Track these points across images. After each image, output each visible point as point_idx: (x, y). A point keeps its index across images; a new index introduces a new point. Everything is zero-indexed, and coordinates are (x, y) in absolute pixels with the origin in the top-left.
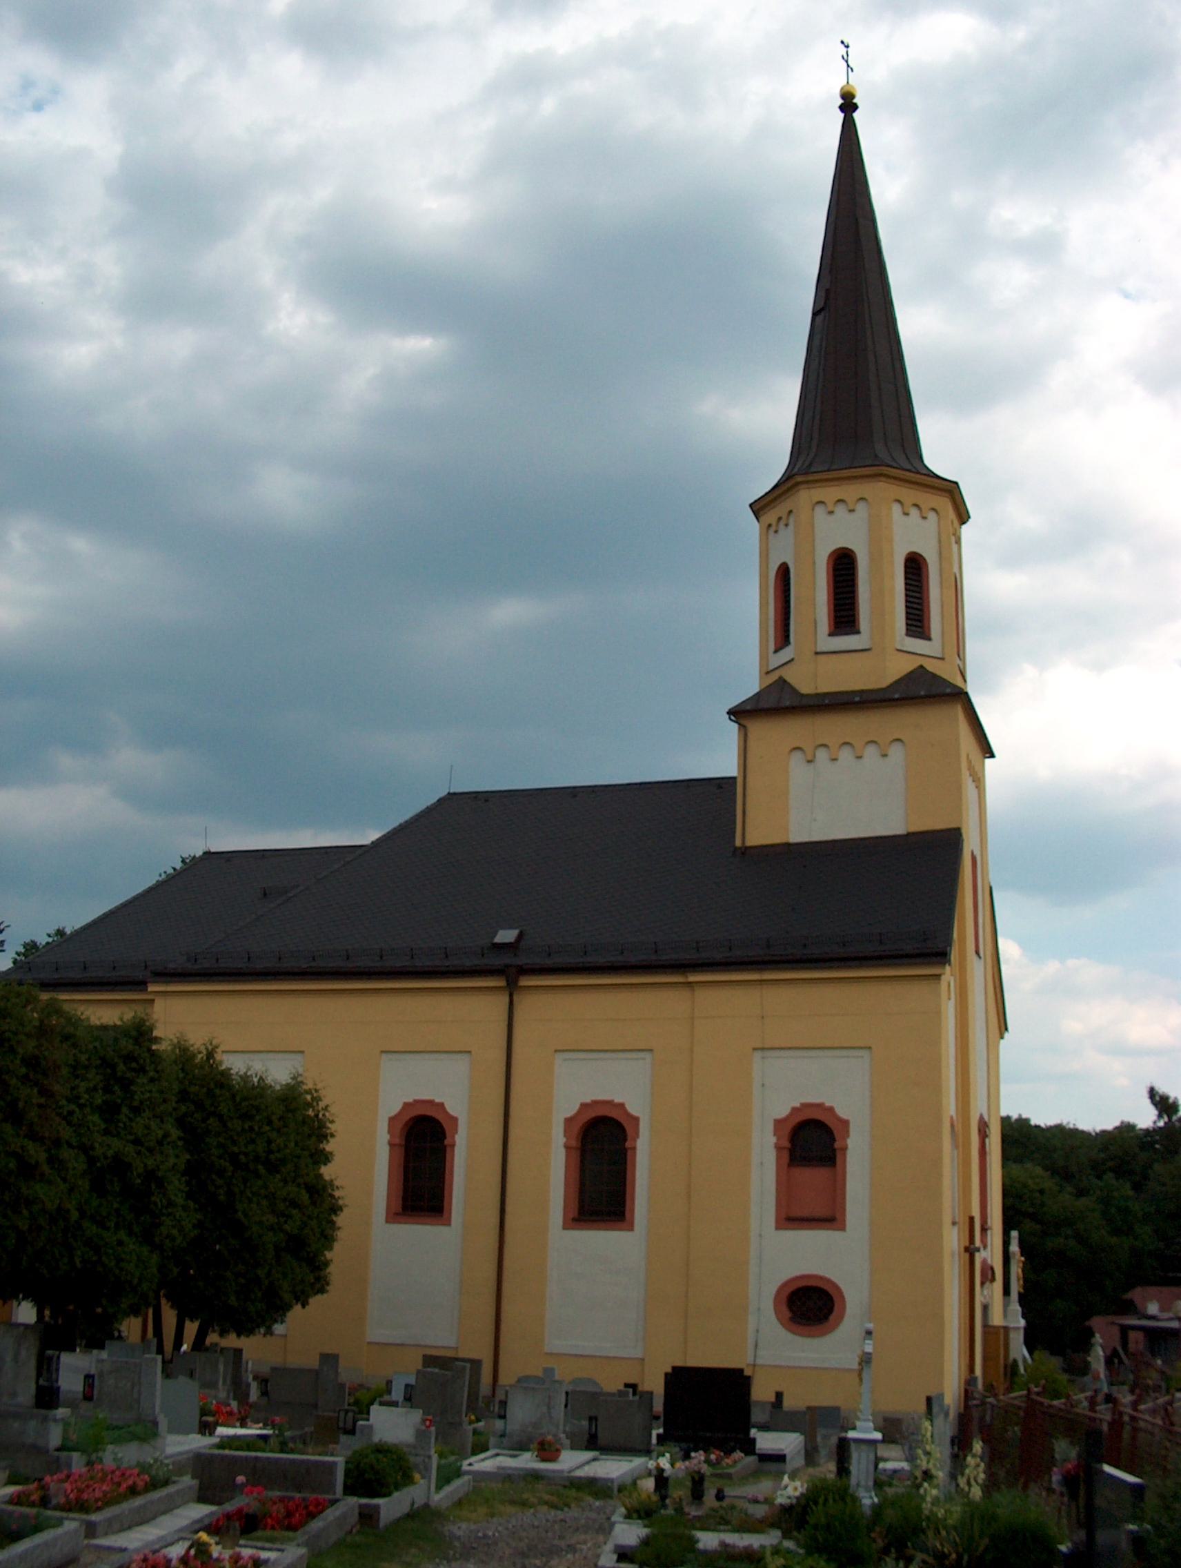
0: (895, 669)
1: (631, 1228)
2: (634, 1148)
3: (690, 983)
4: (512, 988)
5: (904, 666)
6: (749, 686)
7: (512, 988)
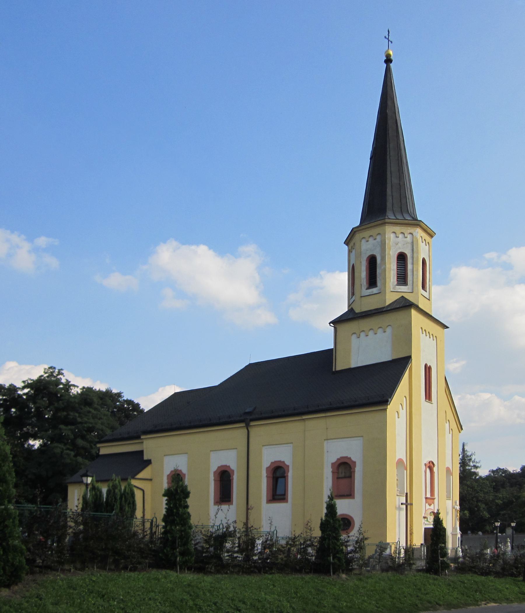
0: (390, 298)
1: (287, 502)
2: (288, 476)
3: (303, 419)
4: (247, 426)
5: (396, 297)
7: (247, 426)
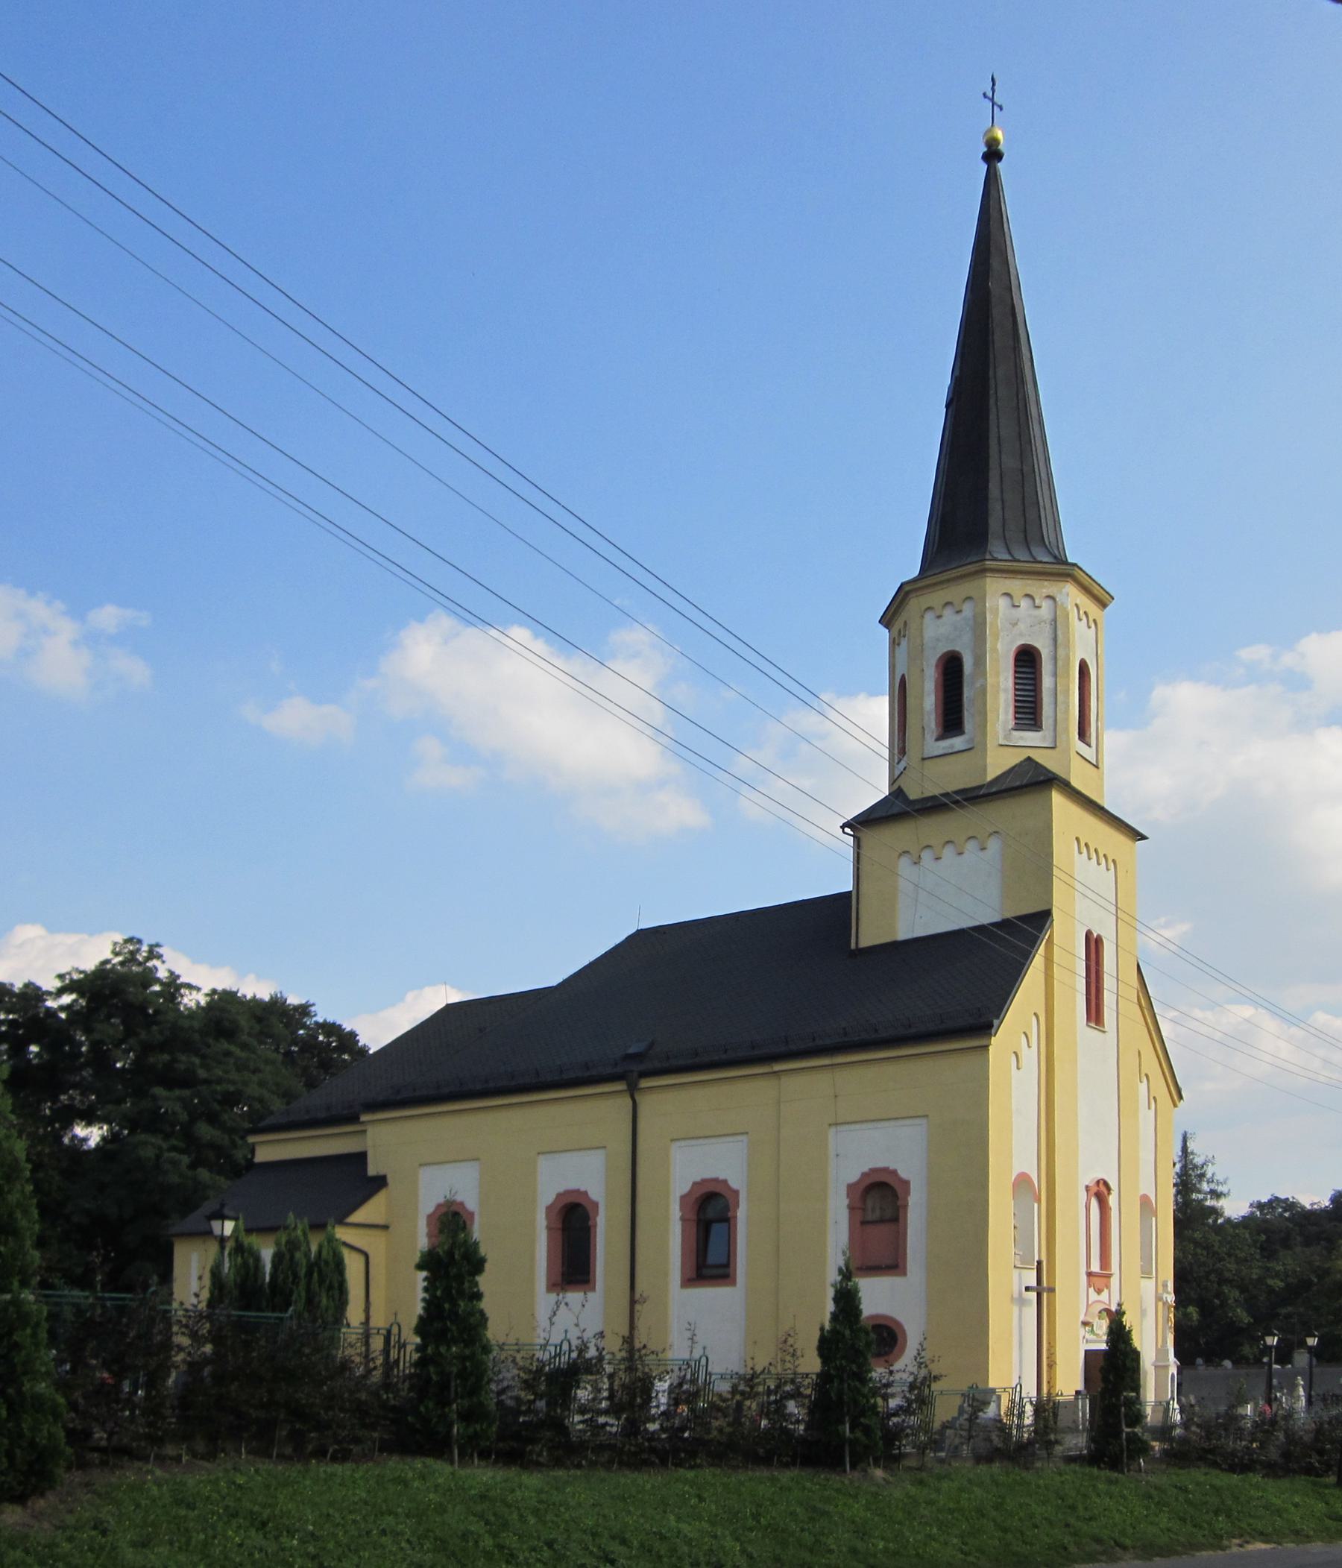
0: (998, 763)
1: (733, 1283)
3: (775, 1072)
4: (633, 1090)
6: (876, 789)
7: (633, 1090)
